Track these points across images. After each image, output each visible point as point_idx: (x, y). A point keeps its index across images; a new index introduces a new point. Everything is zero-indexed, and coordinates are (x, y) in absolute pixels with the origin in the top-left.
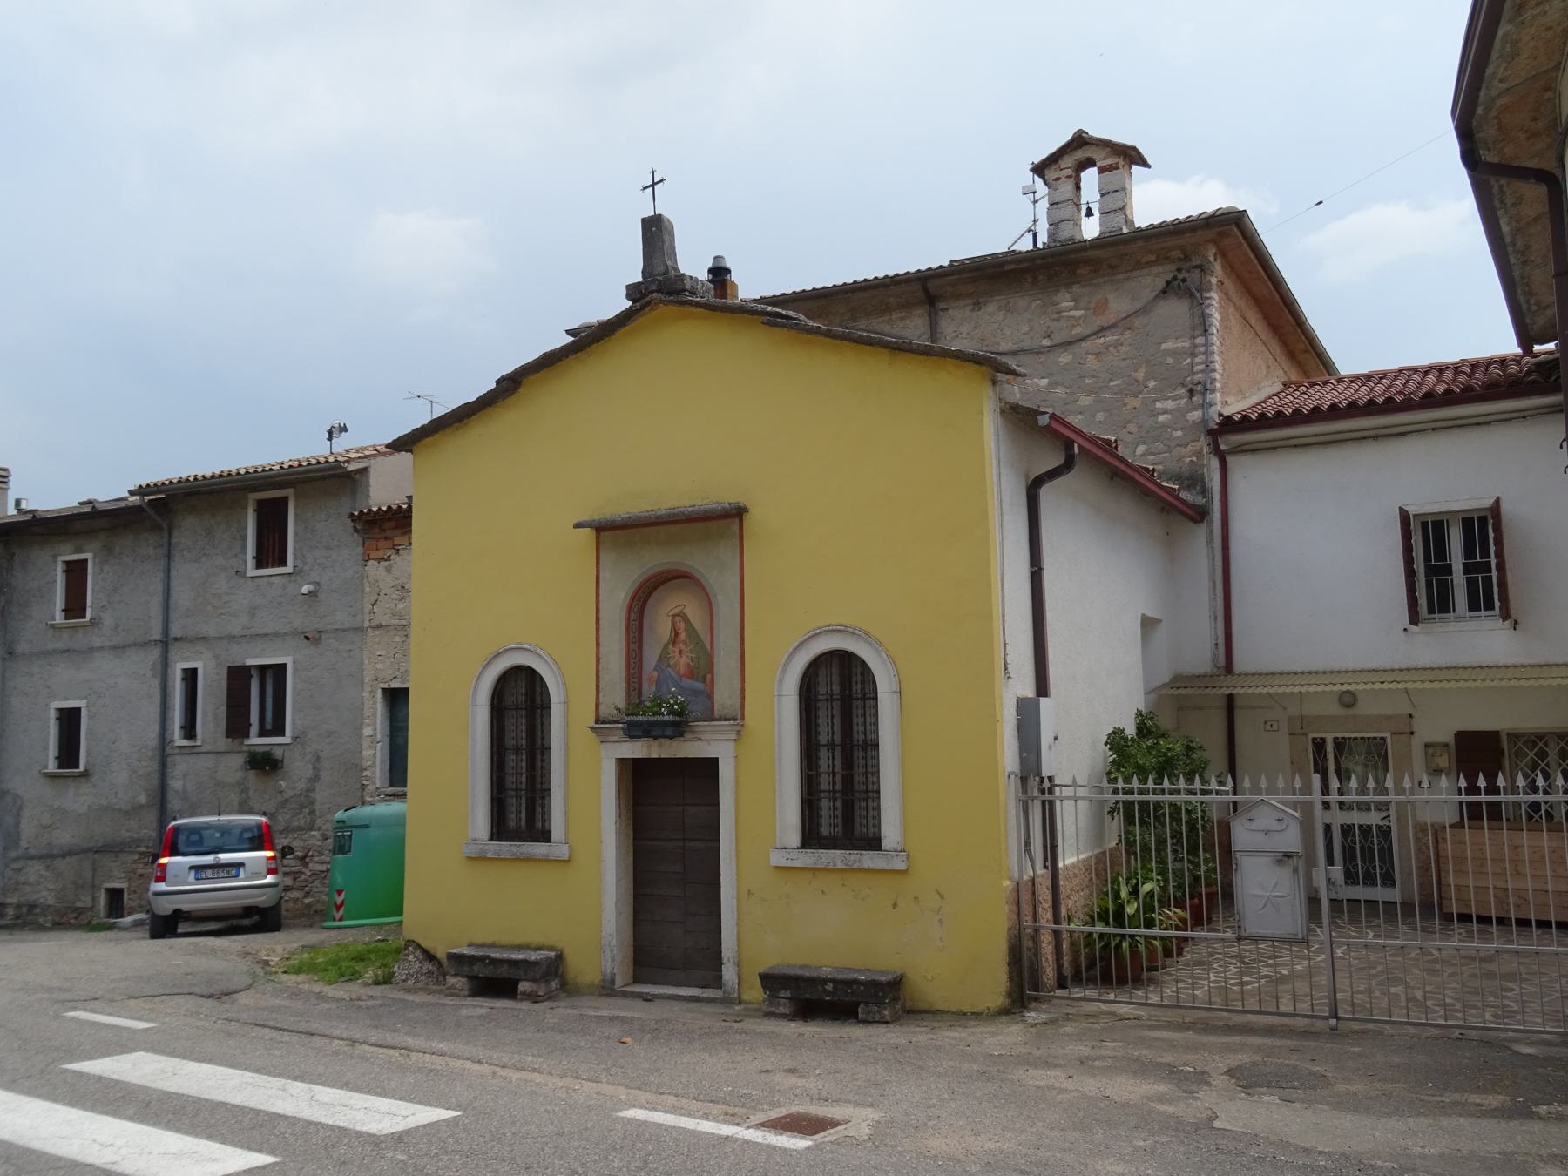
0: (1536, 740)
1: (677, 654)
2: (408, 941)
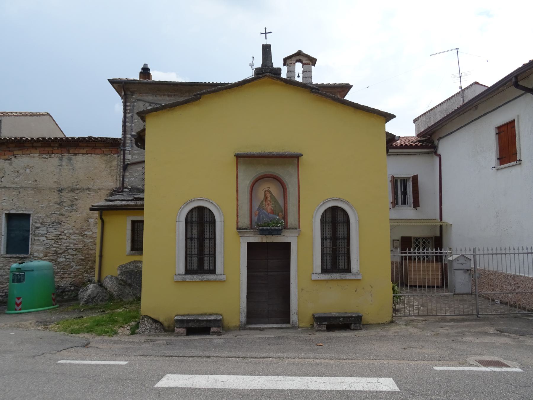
0: (417, 239)
2: (144, 316)
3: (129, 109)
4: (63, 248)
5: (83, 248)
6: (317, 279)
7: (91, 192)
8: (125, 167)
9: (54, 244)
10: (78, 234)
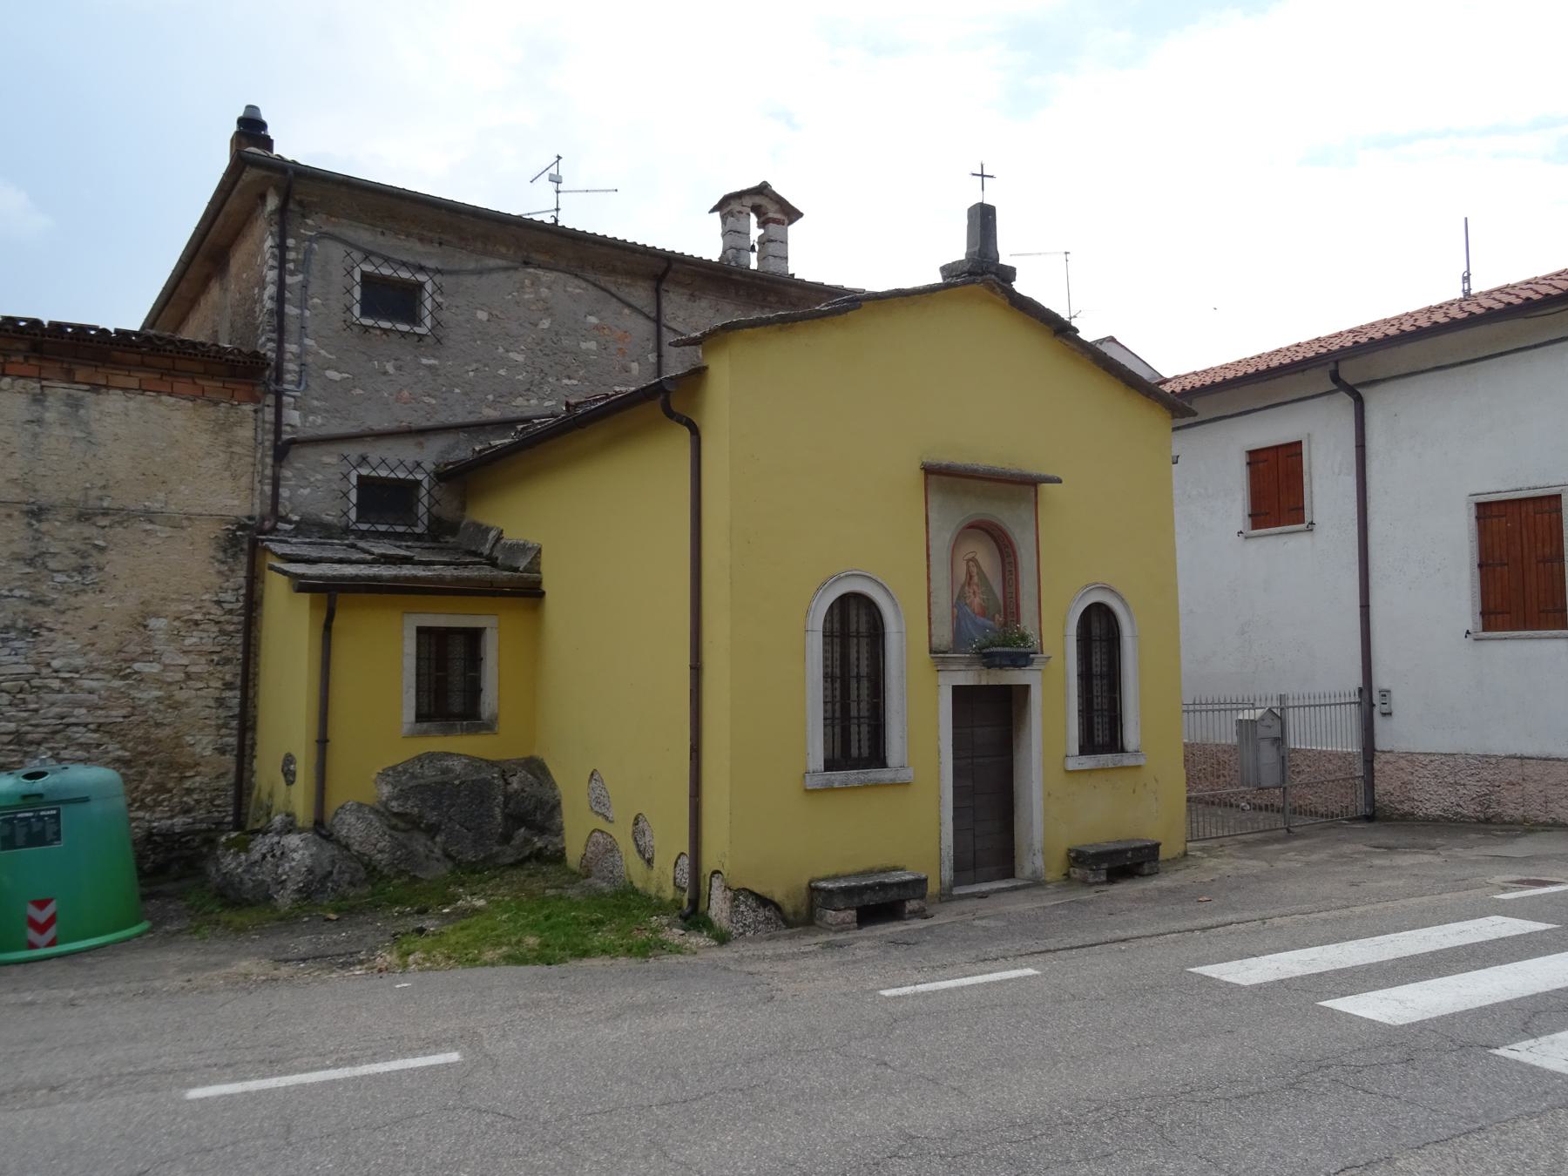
2: (738, 890)
3: (293, 261)
4: (49, 721)
5: (127, 720)
6: (1078, 767)
7: (158, 527)
8: (282, 450)
9: (9, 708)
10: (107, 672)
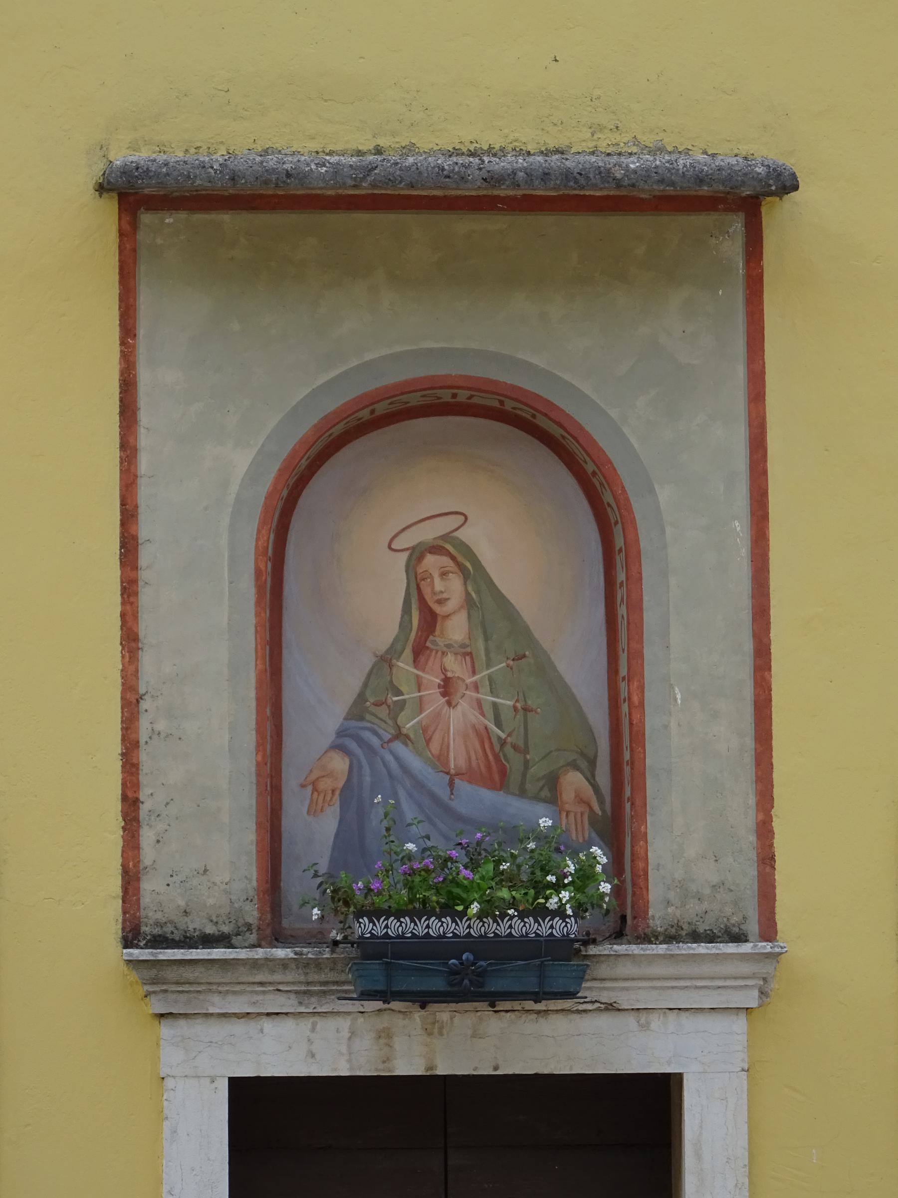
1: (432, 694)
